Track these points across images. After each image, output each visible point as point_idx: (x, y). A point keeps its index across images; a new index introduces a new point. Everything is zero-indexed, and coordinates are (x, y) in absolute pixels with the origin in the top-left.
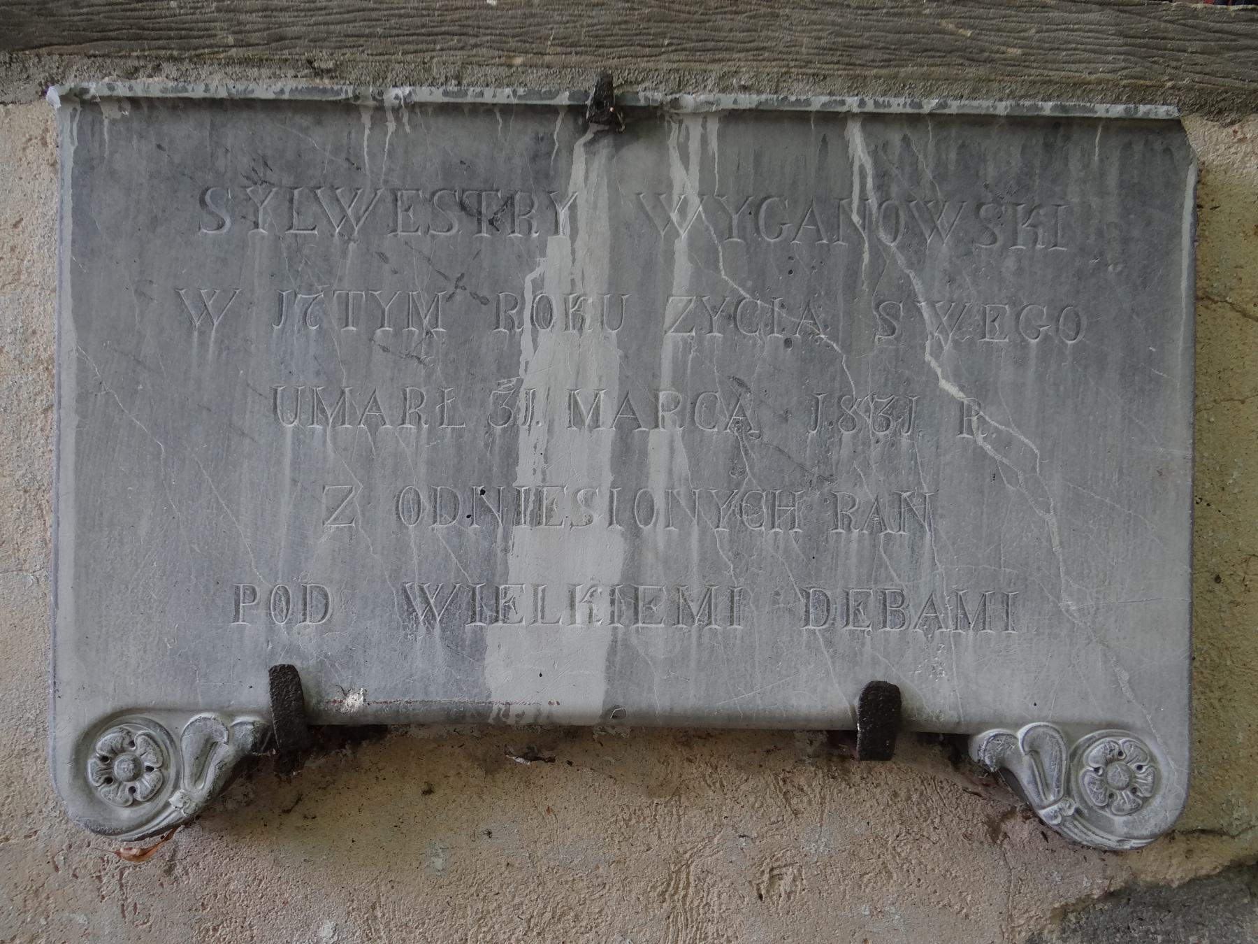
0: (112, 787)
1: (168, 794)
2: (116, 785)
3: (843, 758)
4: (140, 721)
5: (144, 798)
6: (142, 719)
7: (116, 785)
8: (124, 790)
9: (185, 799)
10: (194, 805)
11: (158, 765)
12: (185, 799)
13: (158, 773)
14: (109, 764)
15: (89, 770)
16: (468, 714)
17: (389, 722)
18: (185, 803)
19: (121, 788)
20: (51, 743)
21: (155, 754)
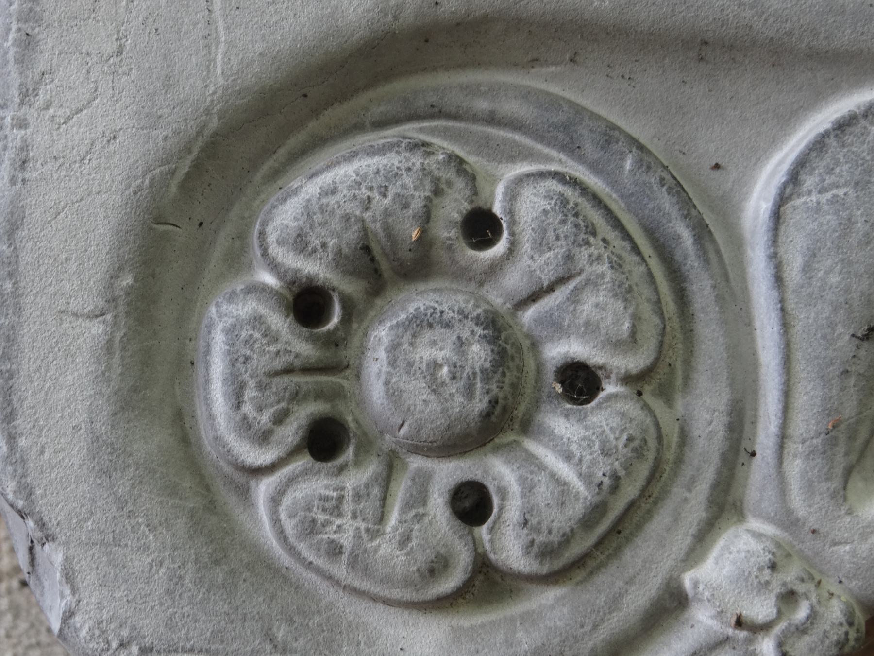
0: (353, 480)
1: (682, 540)
2: (371, 469)
3: (574, 10)
4: (511, 107)
5: (546, 552)
6: (526, 94)
7: (371, 469)
8: (419, 498)
9: (790, 574)
10: (835, 612)
11: (634, 363)
12: (790, 574)
13: (632, 409)
14: (333, 342)
15: (218, 367)
16: (693, 233)
17: (378, 302)
18: (789, 597)
19: (401, 490)
20: (127, 192)
21: (625, 293)
